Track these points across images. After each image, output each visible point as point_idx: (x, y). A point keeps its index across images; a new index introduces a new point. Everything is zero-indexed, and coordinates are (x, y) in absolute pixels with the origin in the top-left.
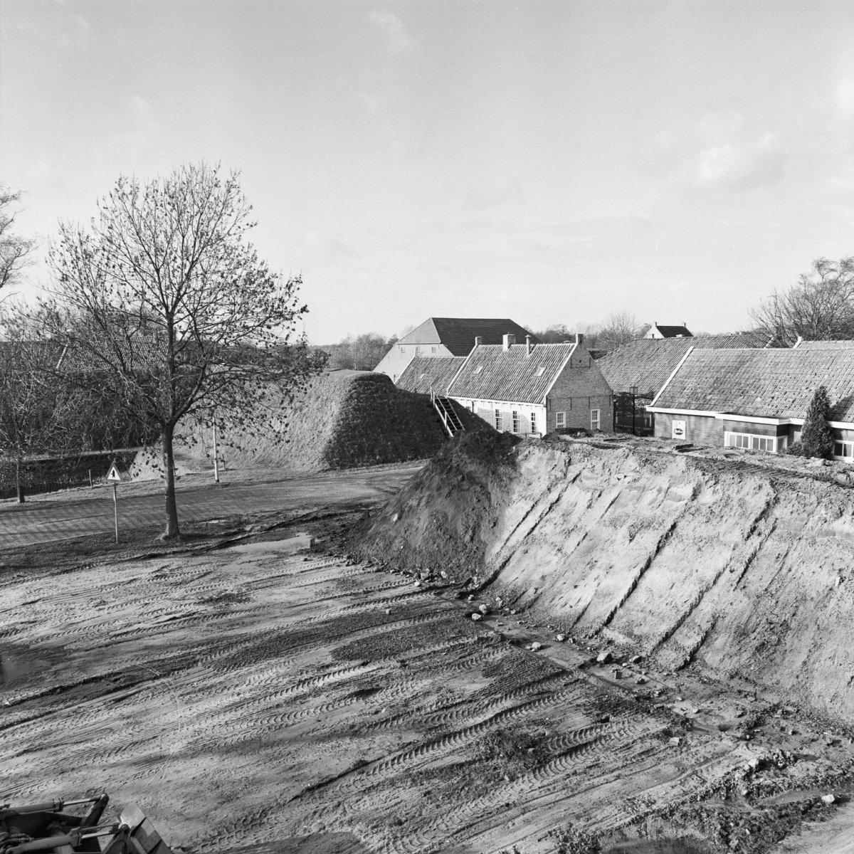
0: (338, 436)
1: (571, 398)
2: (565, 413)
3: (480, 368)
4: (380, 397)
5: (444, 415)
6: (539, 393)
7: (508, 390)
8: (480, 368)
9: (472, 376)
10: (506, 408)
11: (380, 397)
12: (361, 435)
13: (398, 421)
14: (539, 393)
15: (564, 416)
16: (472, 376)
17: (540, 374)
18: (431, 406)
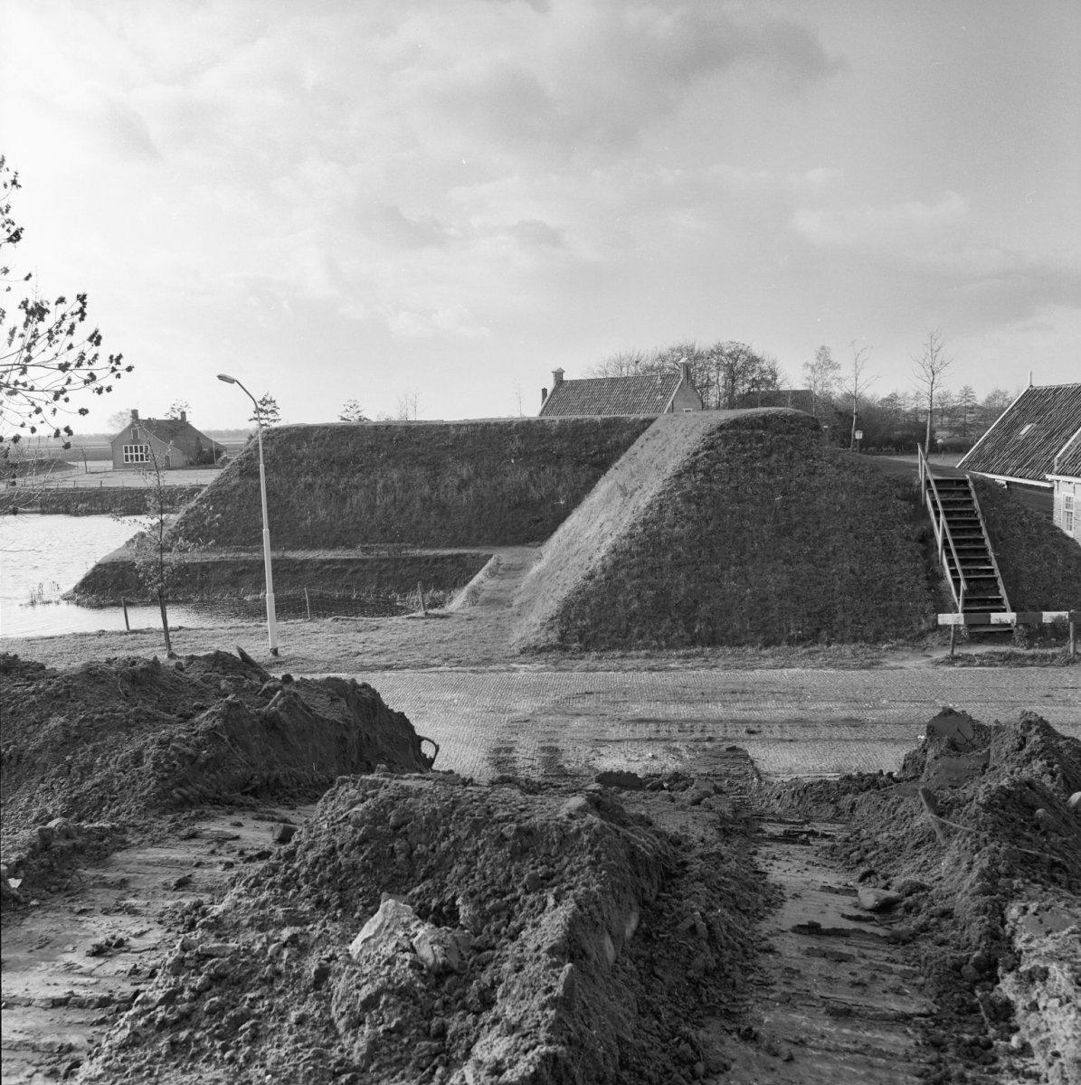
0: (616, 563)
5: (938, 522)
18: (915, 498)
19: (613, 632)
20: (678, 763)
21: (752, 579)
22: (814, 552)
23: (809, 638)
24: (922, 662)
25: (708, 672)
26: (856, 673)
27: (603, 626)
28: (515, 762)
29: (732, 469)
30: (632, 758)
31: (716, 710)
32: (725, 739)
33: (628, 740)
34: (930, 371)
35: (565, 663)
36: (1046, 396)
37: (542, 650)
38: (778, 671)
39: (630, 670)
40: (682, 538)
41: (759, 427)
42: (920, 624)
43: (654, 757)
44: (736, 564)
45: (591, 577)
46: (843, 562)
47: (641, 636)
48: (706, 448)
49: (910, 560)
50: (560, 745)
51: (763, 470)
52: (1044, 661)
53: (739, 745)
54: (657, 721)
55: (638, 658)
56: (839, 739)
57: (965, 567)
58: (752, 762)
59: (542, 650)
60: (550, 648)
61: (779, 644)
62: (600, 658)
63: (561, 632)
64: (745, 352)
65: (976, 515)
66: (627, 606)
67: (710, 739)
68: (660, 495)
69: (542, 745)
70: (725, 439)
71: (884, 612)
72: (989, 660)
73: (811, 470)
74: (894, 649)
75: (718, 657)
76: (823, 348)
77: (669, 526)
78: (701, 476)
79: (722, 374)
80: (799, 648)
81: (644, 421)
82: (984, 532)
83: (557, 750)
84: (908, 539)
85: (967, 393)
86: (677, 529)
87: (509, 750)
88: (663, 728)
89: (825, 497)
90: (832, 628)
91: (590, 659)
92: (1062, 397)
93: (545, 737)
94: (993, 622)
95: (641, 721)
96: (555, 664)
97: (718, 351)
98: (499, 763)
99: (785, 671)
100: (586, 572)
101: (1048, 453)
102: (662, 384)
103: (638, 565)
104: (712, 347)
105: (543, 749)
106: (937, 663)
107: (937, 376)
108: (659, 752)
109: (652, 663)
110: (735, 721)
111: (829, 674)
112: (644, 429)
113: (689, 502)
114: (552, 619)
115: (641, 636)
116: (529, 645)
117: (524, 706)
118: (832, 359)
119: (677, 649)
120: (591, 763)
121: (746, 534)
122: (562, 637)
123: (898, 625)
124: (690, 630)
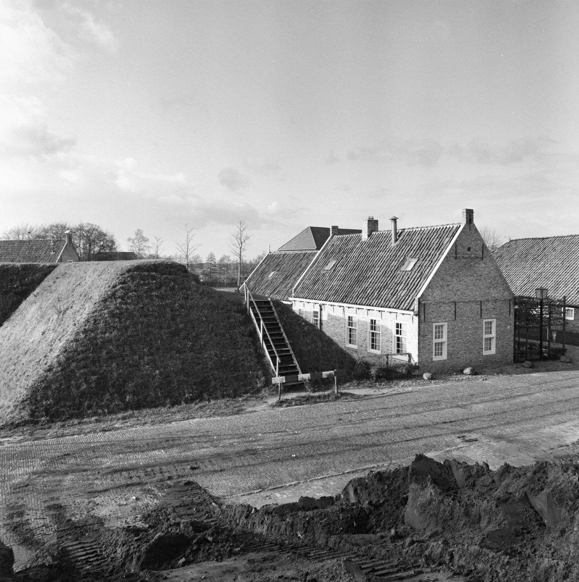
0: (68, 359)
1: (455, 303)
2: (446, 324)
3: (332, 263)
4: (162, 298)
5: (259, 325)
6: (408, 295)
7: (364, 291)
8: (332, 263)
9: (322, 272)
10: (362, 315)
11: (162, 298)
12: (111, 358)
13: (183, 334)
14: (408, 295)
15: (445, 330)
16: (322, 272)
17: (409, 268)
18: (244, 311)
19: (70, 407)
20: (155, 501)
21: (159, 364)
22: (193, 345)
23: (198, 397)
24: (264, 406)
25: (143, 428)
26: (233, 417)
27: (62, 403)
28: (29, 524)
29: (138, 296)
30: (122, 503)
31: (161, 454)
32: (179, 477)
33: (112, 488)
34: (240, 242)
35: (39, 433)
36: (279, 258)
37: (18, 425)
38: (187, 422)
39: (89, 432)
40: (111, 340)
41: (152, 270)
42: (257, 383)
43: (137, 499)
44: (147, 355)
45: (50, 370)
46: (211, 350)
47: (90, 407)
48: (121, 283)
49: (246, 347)
50: (62, 501)
51: (157, 296)
52: (325, 398)
53: (191, 479)
54: (126, 470)
55: (91, 423)
56: (249, 465)
57: (277, 349)
58: (205, 491)
59: (18, 425)
60: (25, 423)
61: (180, 404)
62: (63, 426)
63: (31, 410)
64: (97, 230)
65: (276, 320)
66: (78, 388)
67: (170, 478)
68: (93, 313)
69: (46, 505)
70: (133, 278)
71: (237, 379)
72: (300, 401)
73: (186, 296)
74: (246, 400)
75: (145, 416)
76: (139, 231)
77: (102, 333)
78: (119, 300)
79: (82, 242)
80: (193, 405)
81: (50, 267)
82: (282, 330)
83: (61, 507)
84: (243, 335)
85: (212, 257)
86: (107, 335)
87: (21, 514)
88: (133, 474)
89: (195, 312)
90: (209, 391)
91: (56, 428)
92: (288, 258)
93: (46, 497)
94: (299, 379)
95: (116, 471)
96: (31, 434)
97: (81, 229)
98: (15, 528)
99: (191, 421)
100: (46, 367)
101: (286, 287)
102: (54, 245)
103: (83, 359)
104: (78, 226)
105: (49, 508)
106: (273, 406)
107: (244, 244)
108: (138, 494)
109: (102, 426)
110: (179, 462)
111: (218, 420)
112: (50, 272)
113: (114, 317)
114: (23, 401)
115: (90, 407)
116: (7, 422)
117: (20, 473)
118: (144, 236)
119: (116, 413)
120: (92, 513)
121: (152, 337)
122: (32, 414)
123: (245, 385)
124: (123, 400)
